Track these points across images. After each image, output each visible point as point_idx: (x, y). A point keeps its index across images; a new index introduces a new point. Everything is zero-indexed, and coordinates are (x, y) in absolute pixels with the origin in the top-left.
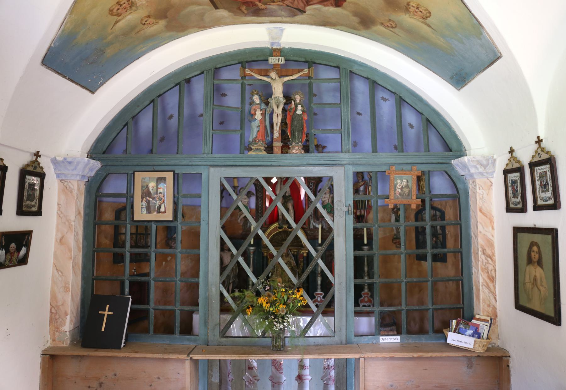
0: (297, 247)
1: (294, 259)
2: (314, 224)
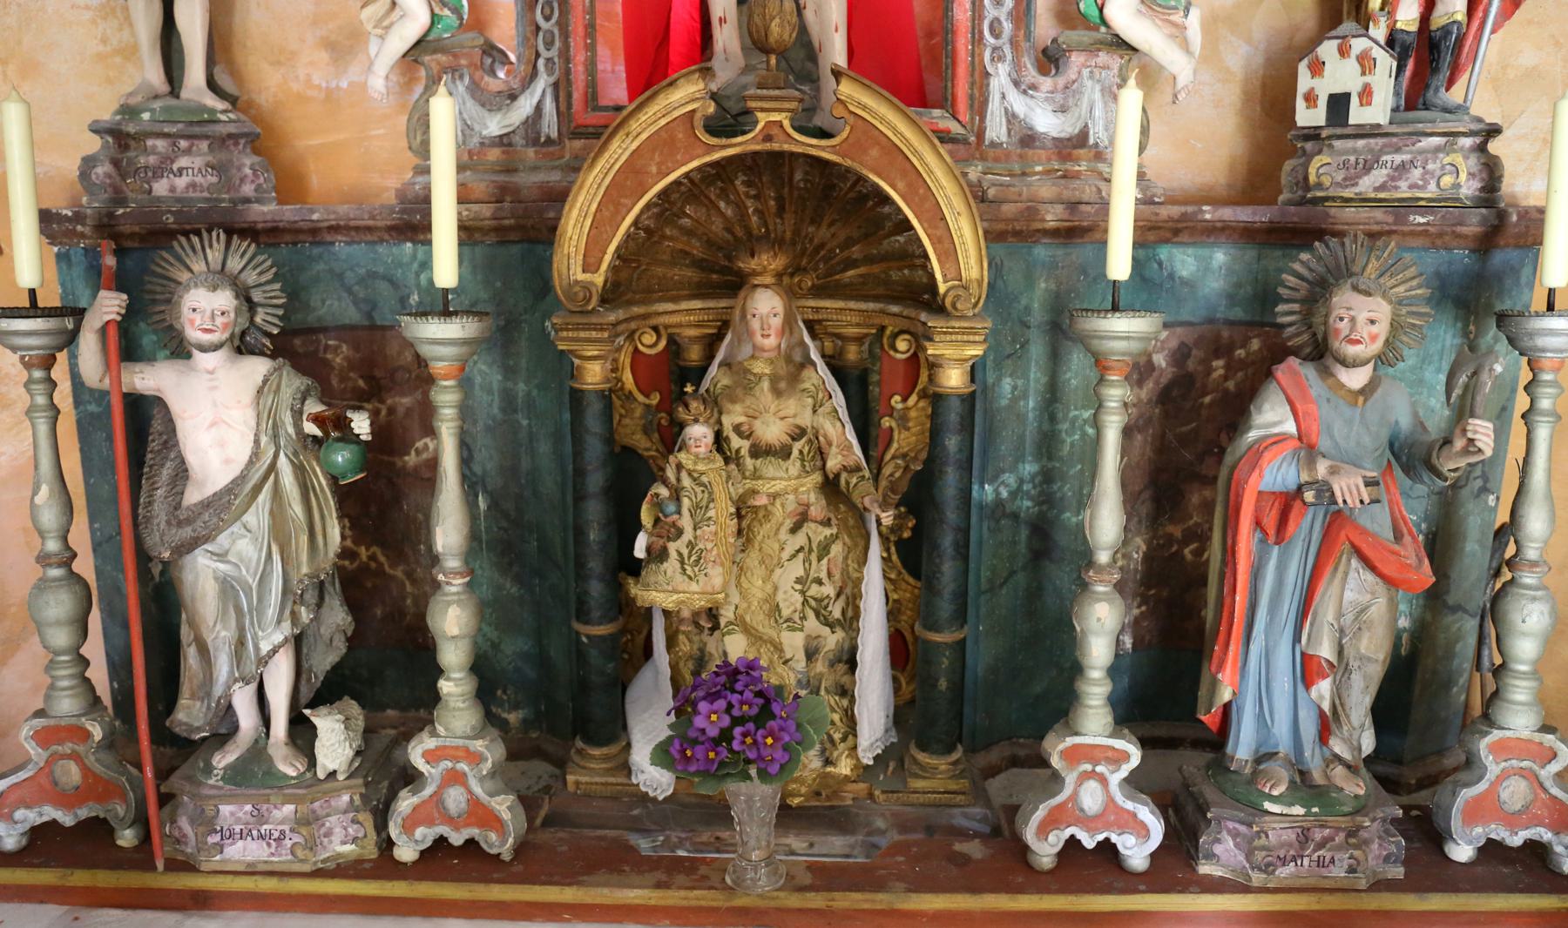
0: (871, 306)
1: (843, 413)
2: (1018, 103)
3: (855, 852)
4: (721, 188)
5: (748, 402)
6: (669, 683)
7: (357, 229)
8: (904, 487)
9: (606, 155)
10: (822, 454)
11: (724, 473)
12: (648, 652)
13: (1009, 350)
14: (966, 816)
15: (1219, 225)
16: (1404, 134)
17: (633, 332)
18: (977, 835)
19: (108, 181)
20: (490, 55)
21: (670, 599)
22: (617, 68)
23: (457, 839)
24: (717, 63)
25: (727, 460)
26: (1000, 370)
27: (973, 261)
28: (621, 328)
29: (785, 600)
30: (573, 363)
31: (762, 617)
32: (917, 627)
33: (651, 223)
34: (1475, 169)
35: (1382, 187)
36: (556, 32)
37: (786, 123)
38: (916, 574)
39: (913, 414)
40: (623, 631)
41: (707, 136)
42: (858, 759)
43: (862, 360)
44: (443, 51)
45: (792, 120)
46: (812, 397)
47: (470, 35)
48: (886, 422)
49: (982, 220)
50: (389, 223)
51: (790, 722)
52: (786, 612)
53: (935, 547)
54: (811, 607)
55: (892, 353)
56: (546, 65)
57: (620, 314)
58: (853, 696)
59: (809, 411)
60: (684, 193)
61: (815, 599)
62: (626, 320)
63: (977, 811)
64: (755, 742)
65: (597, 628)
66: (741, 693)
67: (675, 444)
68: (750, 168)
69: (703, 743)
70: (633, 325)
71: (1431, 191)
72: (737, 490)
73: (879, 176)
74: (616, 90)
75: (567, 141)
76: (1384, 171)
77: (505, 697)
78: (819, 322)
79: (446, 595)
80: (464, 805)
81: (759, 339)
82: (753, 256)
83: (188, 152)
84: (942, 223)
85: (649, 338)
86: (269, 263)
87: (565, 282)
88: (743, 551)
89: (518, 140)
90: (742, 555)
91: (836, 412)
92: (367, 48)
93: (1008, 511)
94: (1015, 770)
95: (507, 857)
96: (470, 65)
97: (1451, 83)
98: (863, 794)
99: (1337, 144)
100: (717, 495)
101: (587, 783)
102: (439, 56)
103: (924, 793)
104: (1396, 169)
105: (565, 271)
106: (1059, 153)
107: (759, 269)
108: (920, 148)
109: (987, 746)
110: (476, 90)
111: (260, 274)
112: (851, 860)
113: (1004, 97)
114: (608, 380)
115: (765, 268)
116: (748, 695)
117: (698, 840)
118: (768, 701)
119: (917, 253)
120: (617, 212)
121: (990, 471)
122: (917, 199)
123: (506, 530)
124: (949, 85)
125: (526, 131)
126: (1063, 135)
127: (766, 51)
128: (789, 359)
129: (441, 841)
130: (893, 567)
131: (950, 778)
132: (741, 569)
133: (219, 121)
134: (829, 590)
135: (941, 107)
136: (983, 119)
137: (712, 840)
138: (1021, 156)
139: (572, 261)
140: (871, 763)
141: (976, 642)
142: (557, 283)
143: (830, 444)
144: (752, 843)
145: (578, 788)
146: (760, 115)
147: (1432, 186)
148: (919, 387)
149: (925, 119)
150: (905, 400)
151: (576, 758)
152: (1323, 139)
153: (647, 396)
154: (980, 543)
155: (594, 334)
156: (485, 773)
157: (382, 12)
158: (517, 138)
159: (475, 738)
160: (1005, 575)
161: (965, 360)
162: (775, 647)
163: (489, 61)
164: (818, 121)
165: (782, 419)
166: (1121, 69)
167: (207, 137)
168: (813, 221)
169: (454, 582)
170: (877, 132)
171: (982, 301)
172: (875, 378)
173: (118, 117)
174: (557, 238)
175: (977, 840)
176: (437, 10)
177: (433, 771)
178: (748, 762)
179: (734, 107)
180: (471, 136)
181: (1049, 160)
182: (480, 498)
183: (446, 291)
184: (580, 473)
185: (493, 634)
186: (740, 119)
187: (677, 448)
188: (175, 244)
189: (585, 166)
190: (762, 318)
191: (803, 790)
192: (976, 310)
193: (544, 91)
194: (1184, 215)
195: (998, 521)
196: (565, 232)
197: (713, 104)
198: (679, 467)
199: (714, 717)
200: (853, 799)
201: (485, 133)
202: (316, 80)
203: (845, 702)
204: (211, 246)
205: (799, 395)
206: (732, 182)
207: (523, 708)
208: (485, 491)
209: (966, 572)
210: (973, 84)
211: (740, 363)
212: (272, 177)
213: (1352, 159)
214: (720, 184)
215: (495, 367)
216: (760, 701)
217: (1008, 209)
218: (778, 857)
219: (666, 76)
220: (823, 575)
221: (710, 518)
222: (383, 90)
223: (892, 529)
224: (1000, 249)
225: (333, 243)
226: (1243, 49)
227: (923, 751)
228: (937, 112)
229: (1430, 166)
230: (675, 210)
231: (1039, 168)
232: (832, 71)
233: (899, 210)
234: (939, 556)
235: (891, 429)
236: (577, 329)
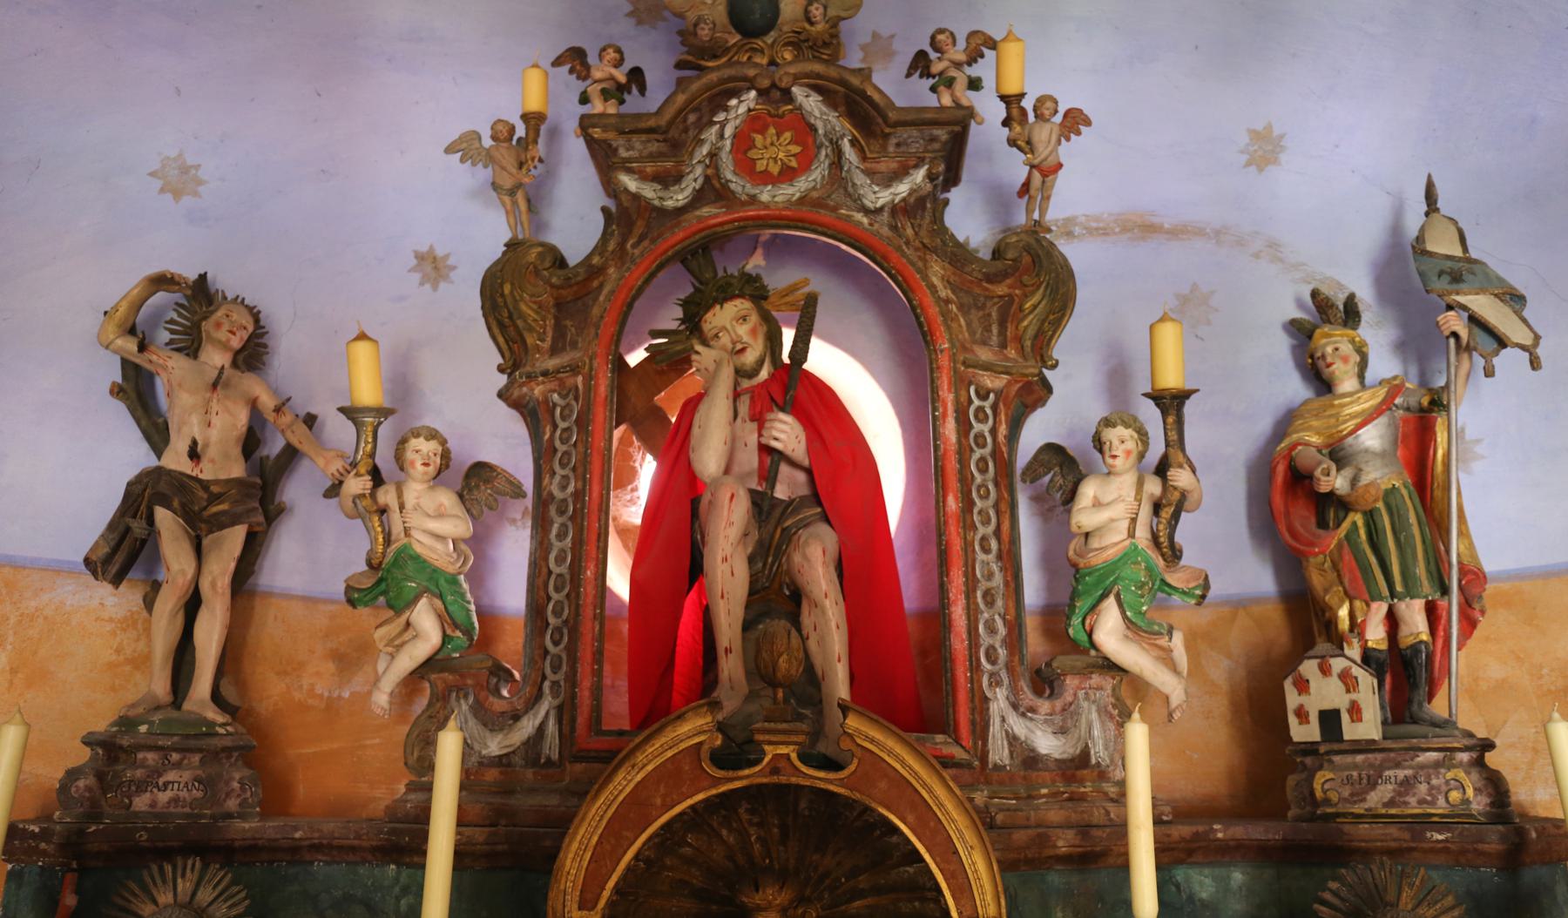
2: (1019, 726)
7: (341, 848)
9: (611, 787)
15: (1232, 843)
16: (1401, 749)
19: (87, 795)
22: (618, 683)
24: (721, 693)
27: (989, 897)
34: (1479, 785)
35: (1391, 803)
36: (564, 657)
37: (794, 756)
41: (714, 769)
44: (452, 670)
47: (480, 656)
49: (994, 850)
50: (374, 843)
56: (551, 688)
71: (1441, 807)
73: (888, 808)
74: (618, 705)
75: (567, 764)
76: (1390, 787)
82: (757, 891)
83: (178, 765)
84: (955, 858)
86: (243, 895)
89: (517, 759)
92: (376, 662)
97: (1431, 696)
99: (1337, 759)
104: (1401, 784)
105: (560, 907)
106: (1063, 775)
108: (928, 781)
110: (479, 710)
111: (230, 907)
113: (1003, 720)
124: (951, 711)
125: (527, 752)
126: (1065, 756)
127: (773, 683)
133: (217, 734)
135: (943, 732)
138: (1025, 778)
146: (766, 748)
147: (1441, 801)
152: (1322, 755)
157: (398, 630)
163: (495, 680)
164: (822, 747)
166: (1114, 690)
167: (200, 750)
173: (114, 729)
176: (449, 632)
180: (470, 755)
181: (1054, 782)
188: (145, 873)
193: (547, 713)
194: (1196, 834)
196: (563, 865)
201: (484, 752)
202: (319, 690)
204: (183, 876)
212: (260, 791)
213: (1355, 774)
214: (723, 812)
217: (1020, 837)
222: (386, 706)
225: (312, 863)
226: (1225, 663)
228: (940, 738)
229: (1434, 782)
231: (1044, 791)
232: (839, 705)
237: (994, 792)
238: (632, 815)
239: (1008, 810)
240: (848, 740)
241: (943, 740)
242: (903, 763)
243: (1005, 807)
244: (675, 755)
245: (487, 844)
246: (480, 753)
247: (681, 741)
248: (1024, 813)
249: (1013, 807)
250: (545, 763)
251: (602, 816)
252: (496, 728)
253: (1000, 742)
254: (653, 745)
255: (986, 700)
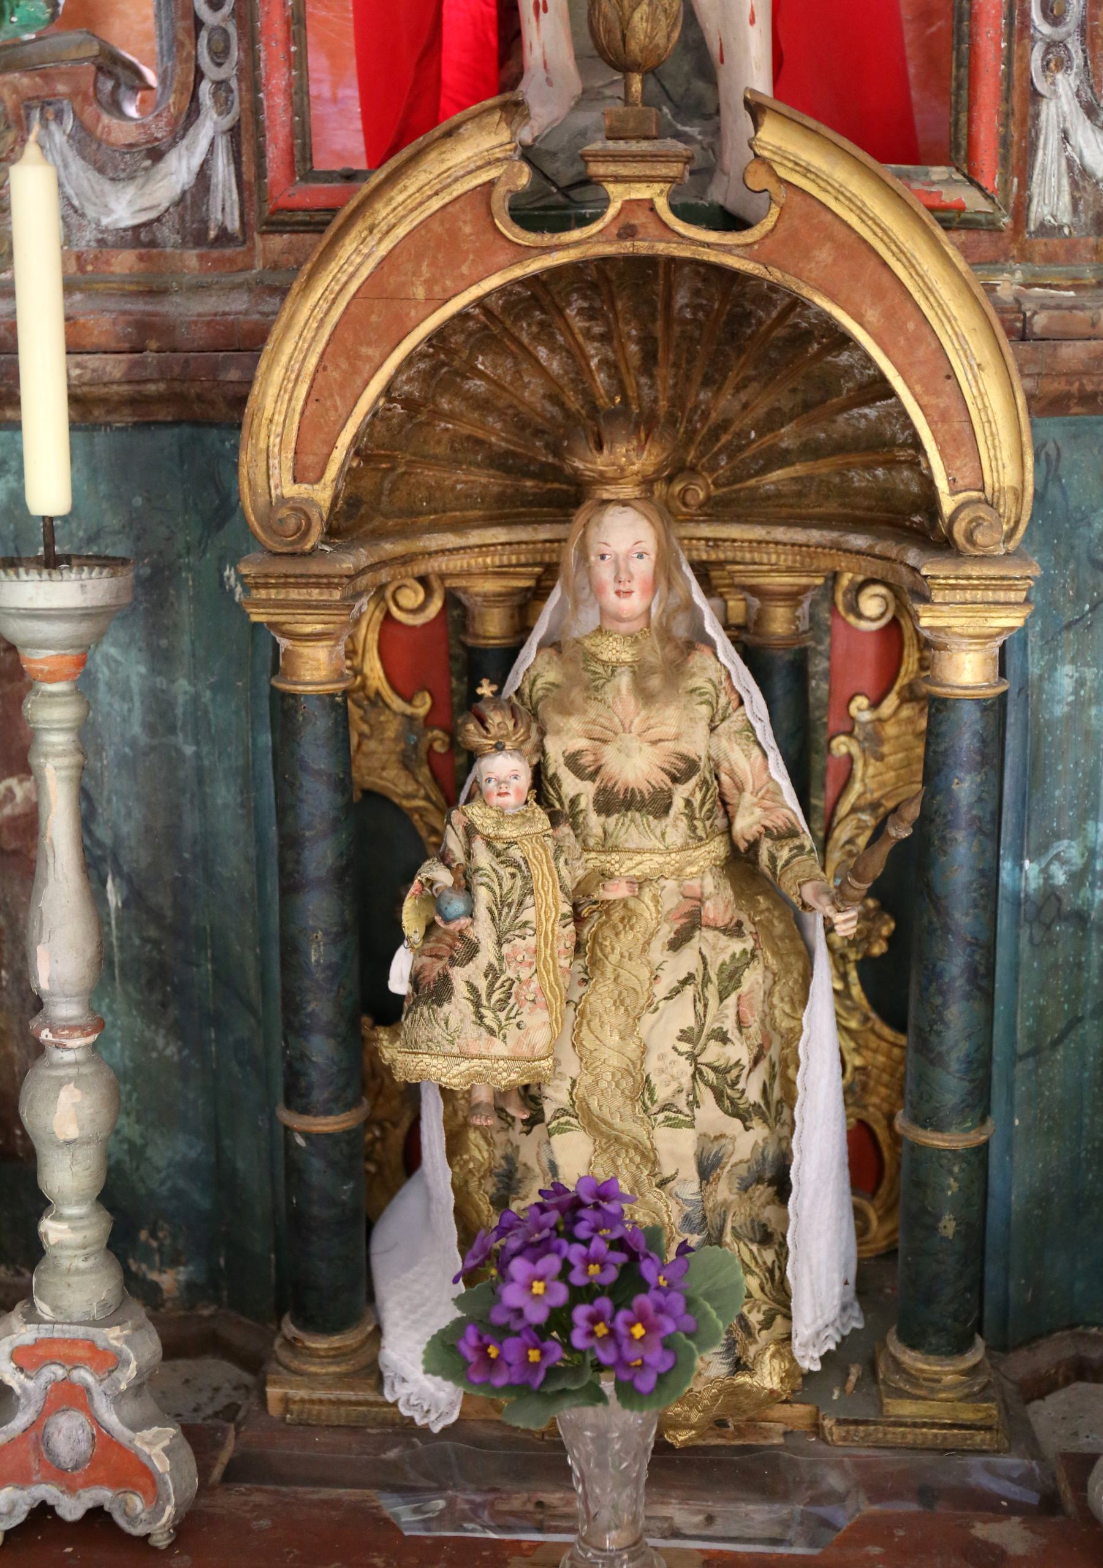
0: (815, 535)
1: (765, 733)
3: (790, 1534)
4: (542, 324)
5: (592, 714)
6: (452, 1218)
8: (877, 865)
9: (333, 267)
10: (725, 806)
11: (550, 842)
12: (411, 1159)
13: (1069, 615)
14: (990, 1469)
17: (382, 588)
18: (1015, 1508)
20: (110, 74)
21: (455, 1070)
22: (342, 92)
23: (71, 1509)
24: (530, 89)
25: (555, 819)
26: (1053, 650)
28: (363, 581)
29: (662, 1071)
30: (276, 646)
31: (619, 1101)
32: (901, 1122)
33: (414, 390)
36: (232, 30)
37: (661, 204)
38: (899, 1024)
39: (890, 730)
40: (368, 1123)
41: (517, 229)
42: (793, 1360)
43: (797, 634)
45: (670, 197)
46: (710, 703)
47: (75, 36)
48: (841, 746)
49: (1023, 375)
51: (674, 1296)
52: (662, 1093)
53: (933, 975)
54: (707, 1084)
55: (852, 619)
56: (215, 95)
57: (362, 557)
58: (783, 1244)
59: (702, 728)
60: (470, 335)
61: (715, 1069)
62: (373, 567)
63: (1012, 1462)
64: (612, 1333)
65: (321, 1120)
66: (587, 1243)
67: (461, 787)
68: (594, 286)
69: (518, 1334)
70: (384, 576)
72: (574, 872)
73: (833, 298)
77: (154, 1244)
78: (721, 564)
79: (53, 1066)
80: (84, 1446)
81: (611, 599)
82: (600, 447)
84: (949, 385)
85: (412, 597)
87: (262, 500)
88: (585, 981)
89: (167, 234)
90: (582, 989)
91: (752, 729)
93: (1067, 908)
94: (1081, 1386)
95: (161, 1541)
96: (72, 96)
98: (803, 1425)
100: (538, 883)
101: (303, 1401)
102: (15, 77)
103: (915, 1425)
105: (261, 479)
107: (610, 471)
108: (908, 245)
109: (1031, 1339)
112: (781, 1550)
113: (1065, 137)
114: (341, 677)
115: (622, 469)
116: (599, 1246)
117: (505, 1507)
118: (634, 1257)
119: (901, 438)
120: (355, 371)
121: (1034, 838)
122: (902, 341)
123: (156, 943)
124: (963, 118)
125: (182, 218)
127: (624, 66)
128: (665, 635)
129: (43, 1512)
130: (852, 1010)
131: (960, 1400)
132: (582, 1014)
134: (739, 1052)
136: (1025, 183)
137: (530, 1507)
139: (274, 462)
140: (817, 1367)
141: (1009, 1147)
142: (247, 502)
143: (740, 789)
144: (606, 1515)
145: (287, 1410)
146: (612, 189)
148: (902, 681)
149: (916, 186)
150: (875, 705)
151: (284, 1355)
153: (408, 700)
154: (1015, 967)
155: (315, 594)
156: (123, 1386)
158: (166, 231)
159: (107, 1322)
160: (1061, 1025)
161: (991, 637)
162: (643, 1156)
163: (109, 85)
164: (717, 194)
165: (654, 743)
168: (707, 382)
169: (70, 1043)
170: (829, 217)
171: (1022, 528)
172: (819, 665)
174: (247, 420)
175: (1016, 1519)
177: (30, 1384)
178: (599, 1367)
179: (566, 174)
180: (80, 228)
182: (110, 885)
183: (49, 522)
184: (291, 842)
185: (132, 1130)
186: (575, 194)
187: (463, 796)
189: (296, 287)
190: (616, 562)
191: (695, 1417)
192: (1012, 546)
193: (212, 144)
195: (1048, 927)
196: (261, 409)
197: (526, 169)
198: (470, 831)
199: (538, 1287)
200: (785, 1434)
201: (105, 221)
203: (769, 1256)
205: (684, 700)
206: (561, 312)
207: (185, 1265)
208: (118, 872)
209: (990, 1021)
210: (1007, 115)
211: (578, 642)
214: (538, 315)
215: (134, 653)
216: (621, 1258)
218: (652, 1542)
219: (436, 123)
220: (730, 1025)
221: (525, 924)
223: (852, 943)
224: (1055, 428)
227: (913, 1347)
228: (938, 172)
230: (456, 363)
232: (747, 102)
233: (868, 359)
234: (942, 993)
235: (850, 758)
236: (286, 585)
237: (1034, 275)
238: (374, 318)
239: (1058, 307)
240: (762, 170)
241: (945, 177)
242: (862, 212)
243: (1052, 303)
244: (444, 207)
245: (129, 382)
246: (98, 224)
247: (456, 180)
248: (1088, 314)
249: (1070, 303)
250: (217, 238)
251: (322, 321)
252: (122, 175)
253: (1054, 180)
254: (405, 187)
255: (1035, 96)
